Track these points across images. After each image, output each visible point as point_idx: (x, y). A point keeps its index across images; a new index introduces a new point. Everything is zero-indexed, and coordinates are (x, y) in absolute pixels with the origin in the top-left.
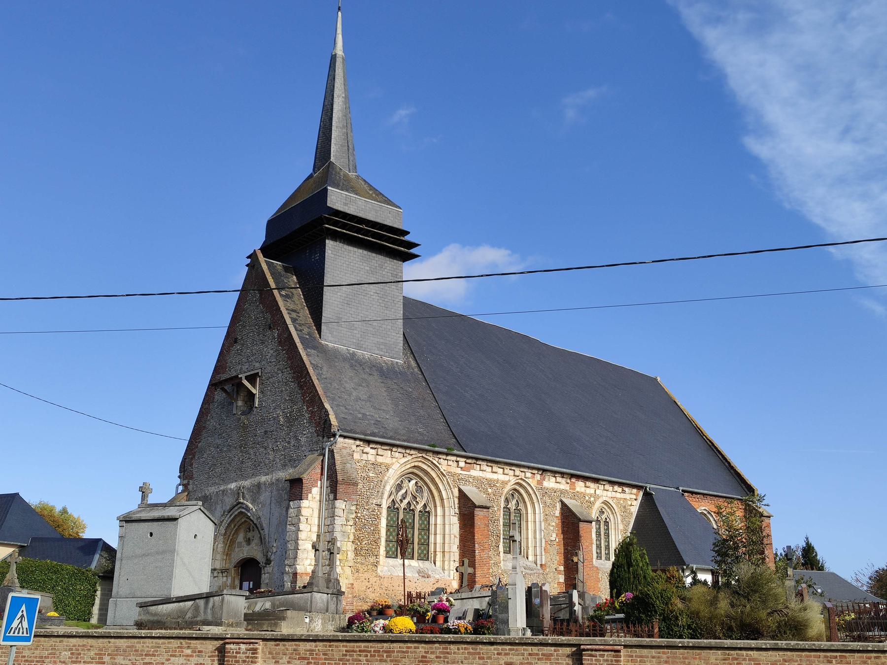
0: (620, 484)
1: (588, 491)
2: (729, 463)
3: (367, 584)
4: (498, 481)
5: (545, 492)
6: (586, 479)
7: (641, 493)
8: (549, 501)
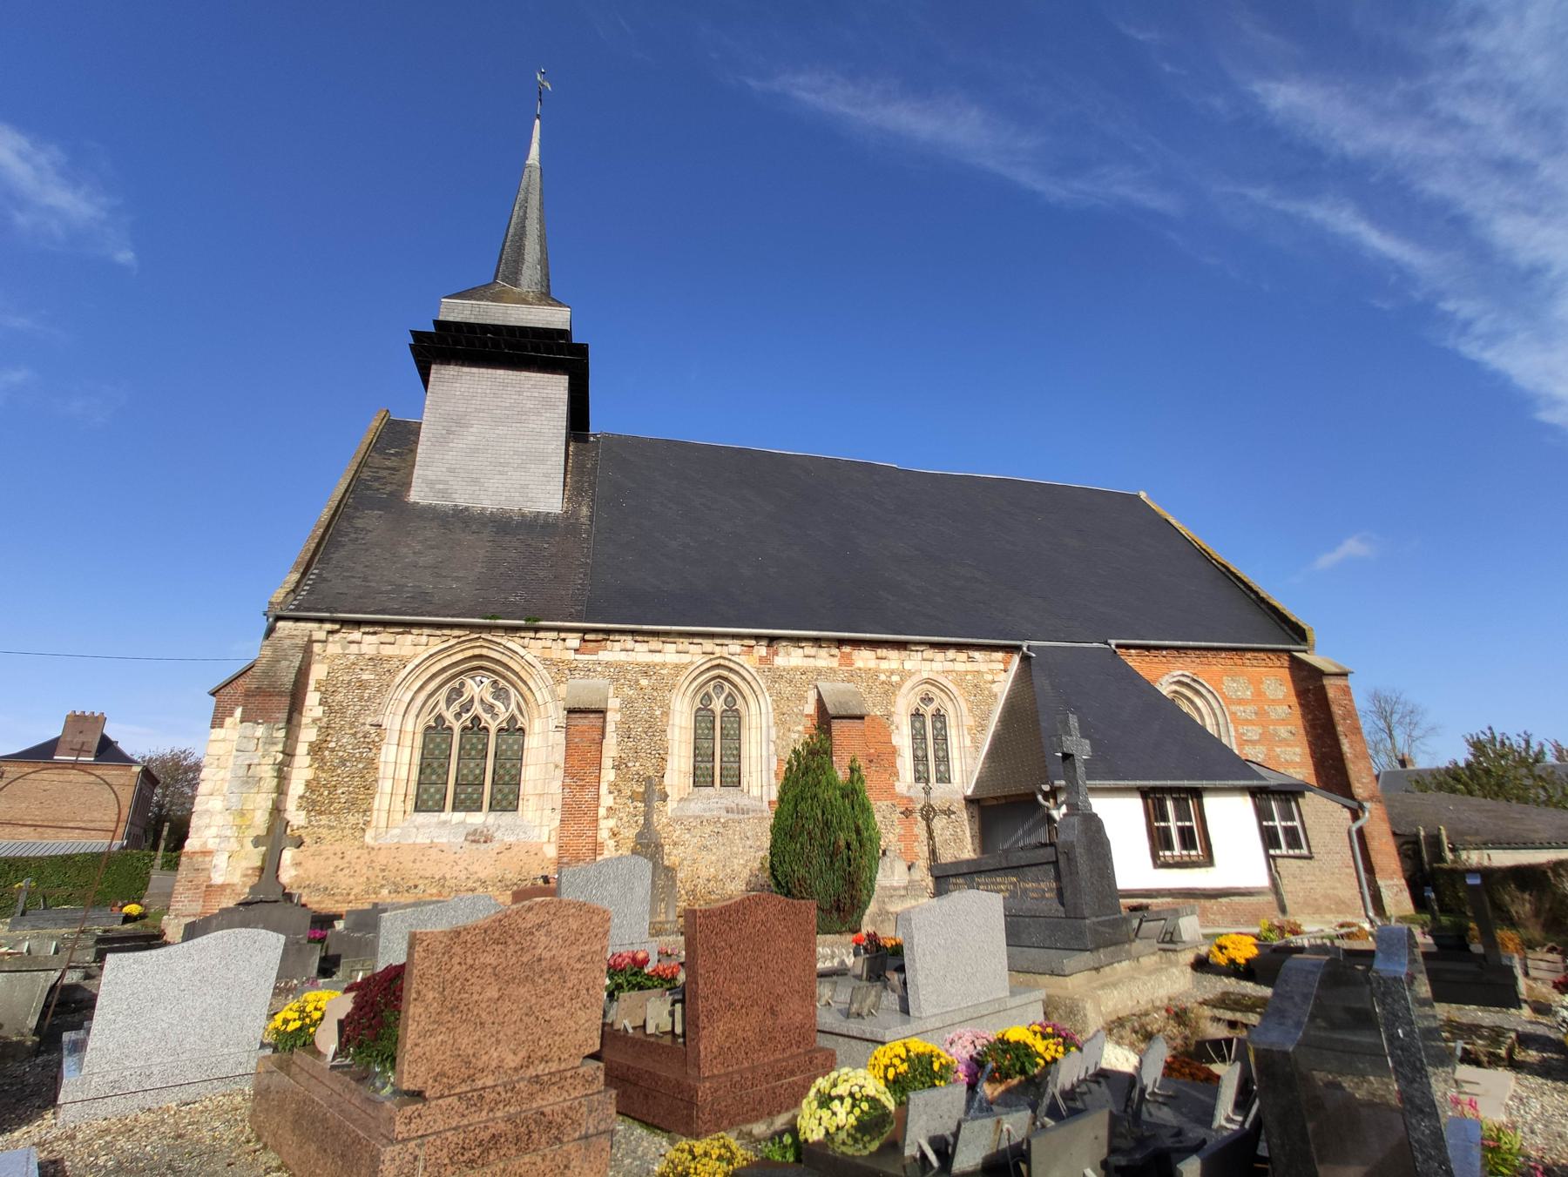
0: (960, 647)
1: (884, 665)
2: (1256, 593)
3: (338, 861)
4: (664, 665)
5: (777, 676)
6: (874, 644)
7: (1016, 659)
8: (788, 690)
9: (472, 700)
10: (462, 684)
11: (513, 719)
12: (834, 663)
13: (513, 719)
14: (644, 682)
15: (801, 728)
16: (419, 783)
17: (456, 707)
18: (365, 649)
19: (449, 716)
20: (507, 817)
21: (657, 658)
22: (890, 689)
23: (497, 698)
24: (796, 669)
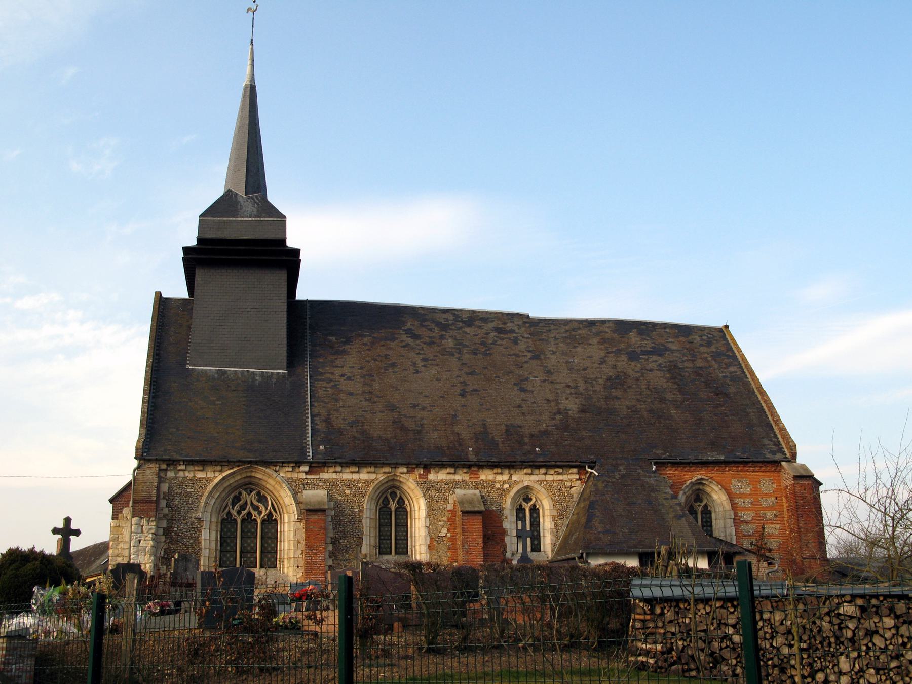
4: (359, 481)
9: (246, 503)
10: (240, 494)
11: (270, 514)
12: (467, 477)
13: (270, 514)
14: (347, 492)
15: (445, 519)
16: (221, 551)
17: (237, 507)
18: (187, 474)
19: (234, 512)
20: (271, 572)
21: (339, 476)
22: (503, 492)
23: (259, 501)
24: (442, 481)
